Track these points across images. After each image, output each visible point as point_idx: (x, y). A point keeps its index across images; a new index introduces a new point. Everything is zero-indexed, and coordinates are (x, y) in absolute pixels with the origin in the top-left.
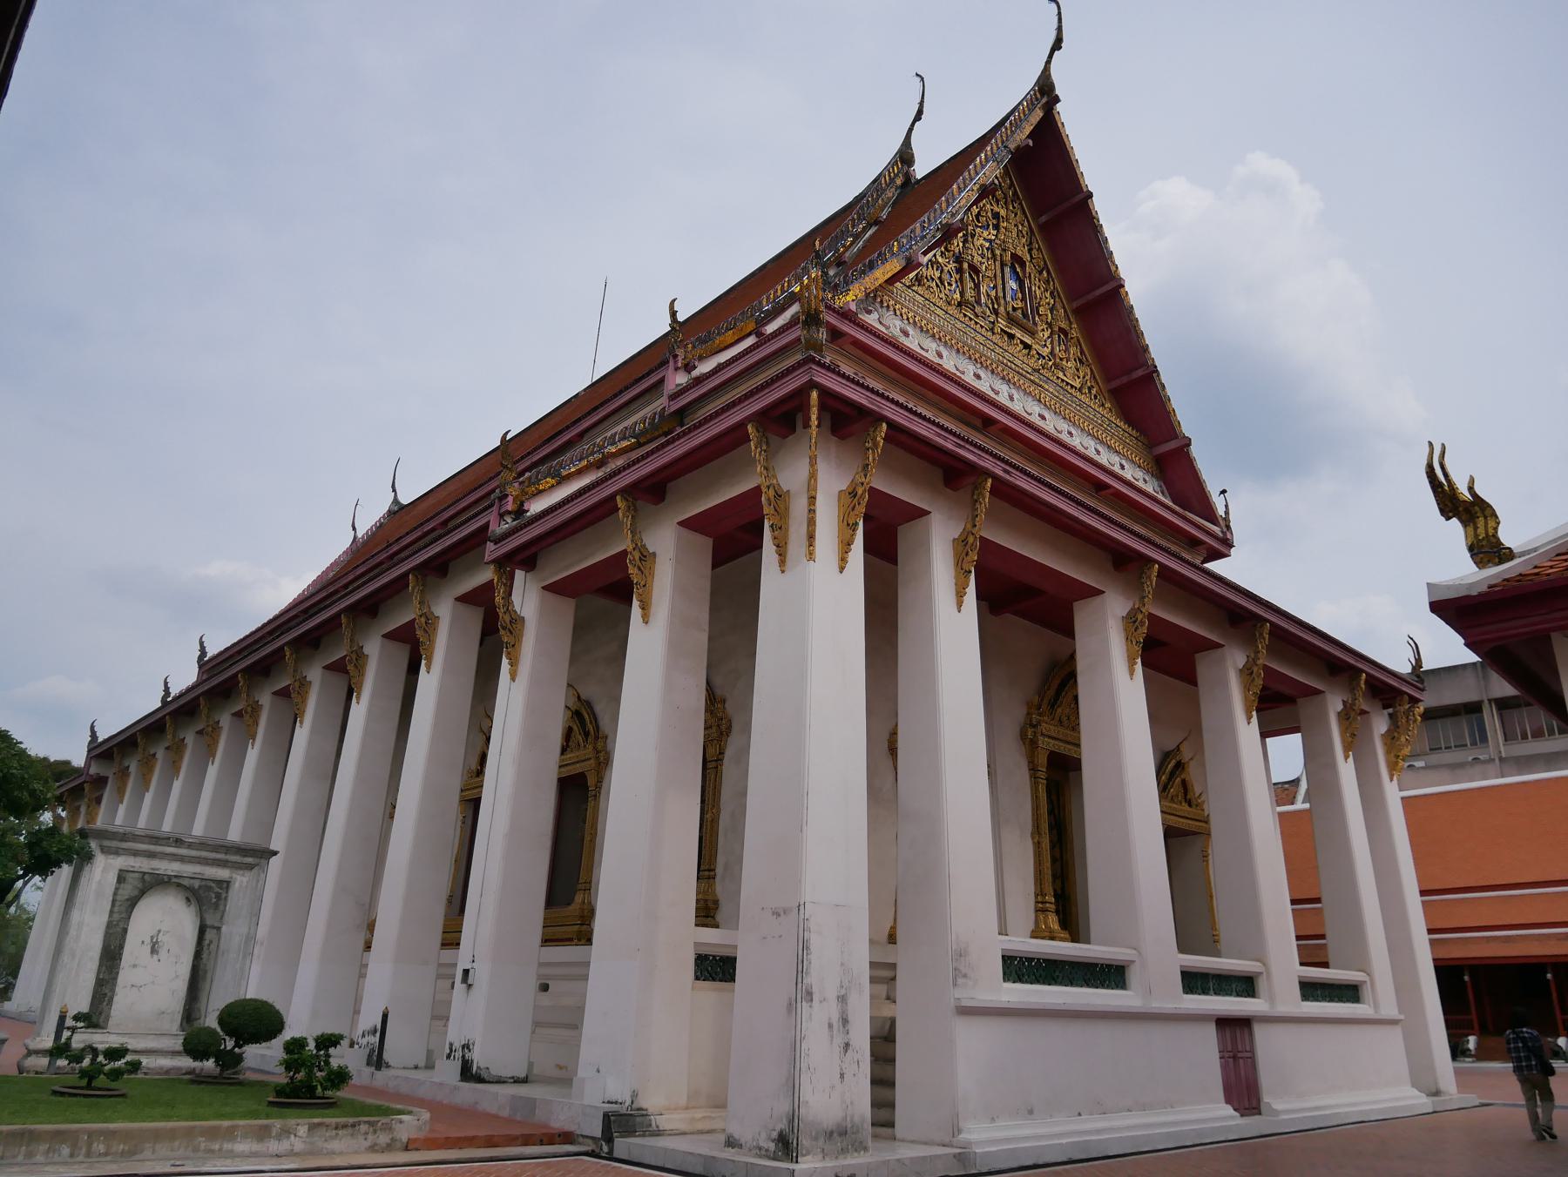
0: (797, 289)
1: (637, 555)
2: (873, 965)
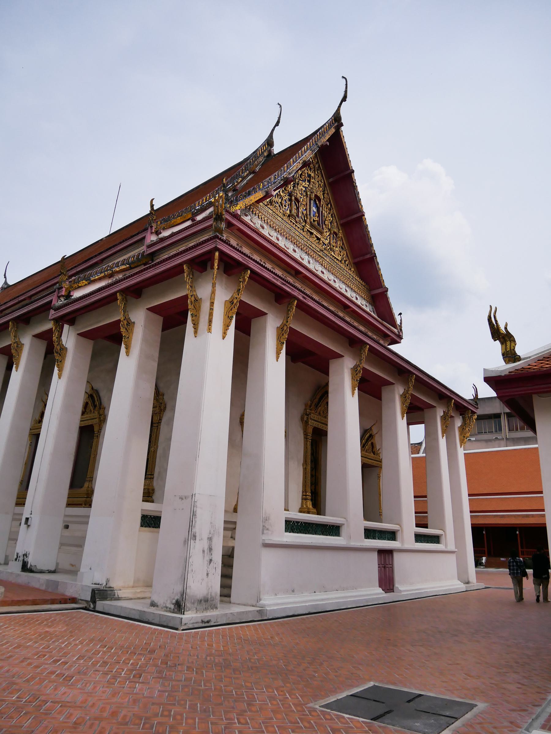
0: (212, 200)
1: (125, 322)
2: (226, 522)
